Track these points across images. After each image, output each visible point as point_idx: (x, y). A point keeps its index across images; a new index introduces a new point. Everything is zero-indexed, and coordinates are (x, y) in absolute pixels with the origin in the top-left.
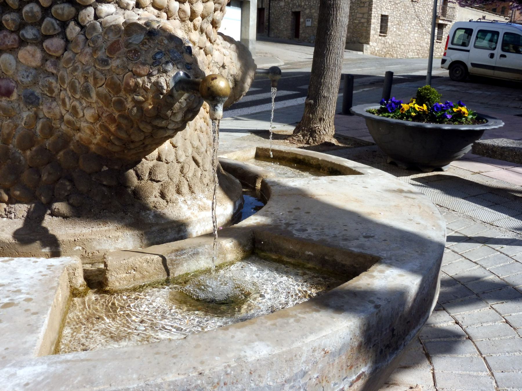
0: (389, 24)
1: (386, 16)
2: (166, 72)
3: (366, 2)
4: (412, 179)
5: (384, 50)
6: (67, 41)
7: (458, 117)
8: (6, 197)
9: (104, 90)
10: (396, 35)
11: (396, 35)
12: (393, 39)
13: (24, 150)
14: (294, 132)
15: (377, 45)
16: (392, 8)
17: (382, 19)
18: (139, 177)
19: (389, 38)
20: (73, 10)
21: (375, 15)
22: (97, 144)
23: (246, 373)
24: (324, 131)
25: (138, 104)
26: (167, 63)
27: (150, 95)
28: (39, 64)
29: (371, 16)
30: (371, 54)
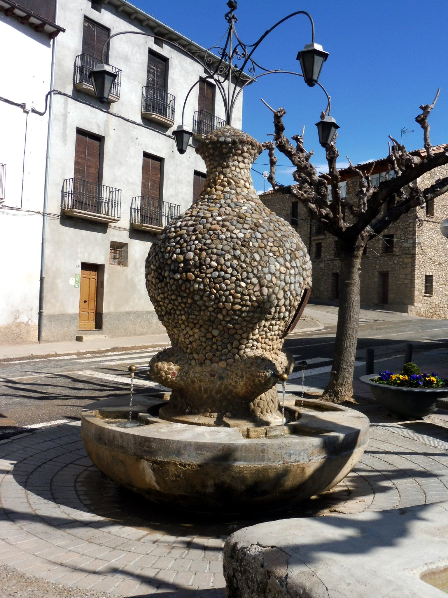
0: (434, 284)
1: (431, 277)
2: (268, 371)
3: (408, 263)
4: (399, 424)
5: (431, 311)
6: (235, 360)
7: (429, 384)
8: (210, 411)
9: (249, 376)
10: (443, 295)
11: (443, 295)
12: (440, 299)
13: (217, 394)
14: (323, 394)
15: (423, 306)
16: (437, 269)
17: (426, 280)
18: (254, 405)
19: (436, 299)
20: (238, 351)
21: (418, 275)
22: (243, 393)
23: (293, 444)
24: (344, 393)
25: (259, 381)
26: (269, 369)
27: (264, 378)
28: (225, 366)
29: (415, 277)
30: (417, 315)
